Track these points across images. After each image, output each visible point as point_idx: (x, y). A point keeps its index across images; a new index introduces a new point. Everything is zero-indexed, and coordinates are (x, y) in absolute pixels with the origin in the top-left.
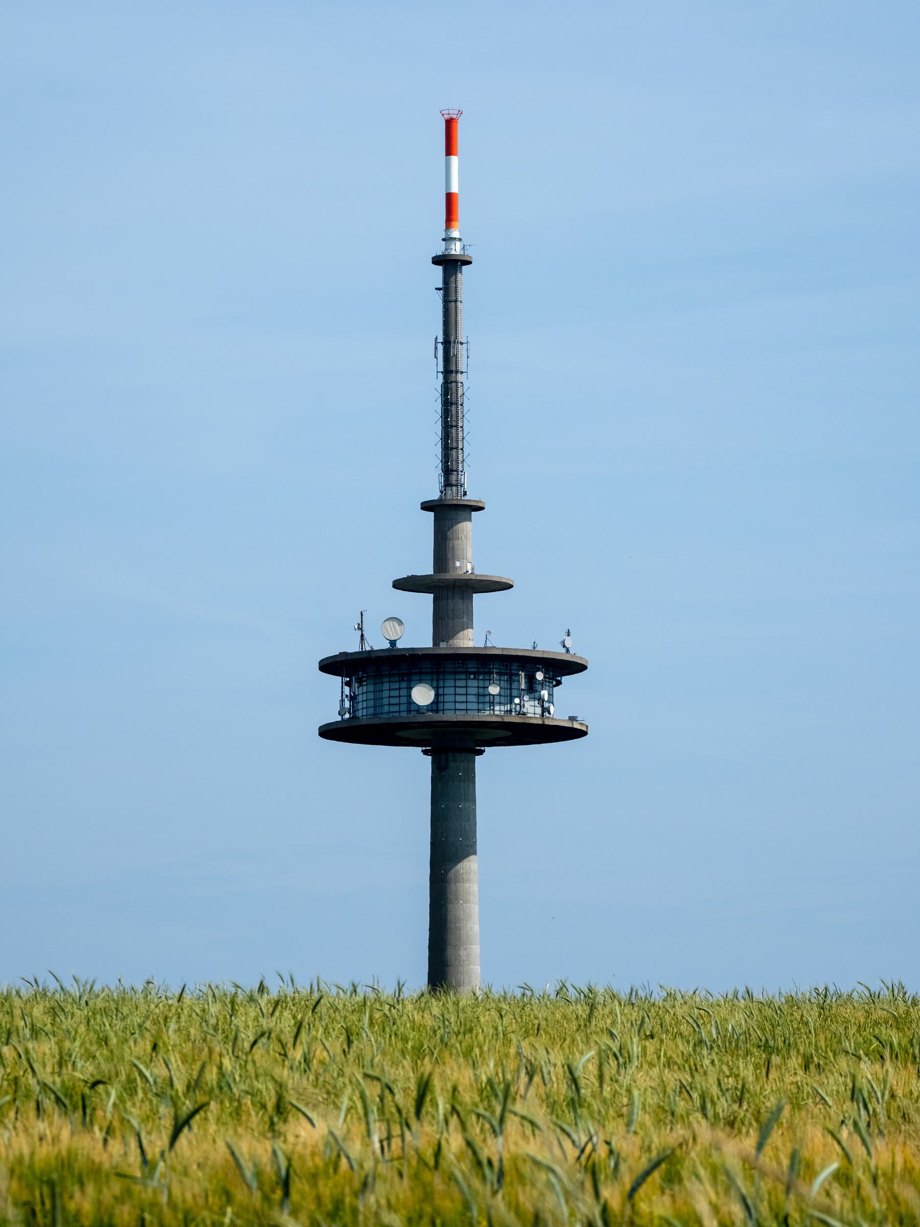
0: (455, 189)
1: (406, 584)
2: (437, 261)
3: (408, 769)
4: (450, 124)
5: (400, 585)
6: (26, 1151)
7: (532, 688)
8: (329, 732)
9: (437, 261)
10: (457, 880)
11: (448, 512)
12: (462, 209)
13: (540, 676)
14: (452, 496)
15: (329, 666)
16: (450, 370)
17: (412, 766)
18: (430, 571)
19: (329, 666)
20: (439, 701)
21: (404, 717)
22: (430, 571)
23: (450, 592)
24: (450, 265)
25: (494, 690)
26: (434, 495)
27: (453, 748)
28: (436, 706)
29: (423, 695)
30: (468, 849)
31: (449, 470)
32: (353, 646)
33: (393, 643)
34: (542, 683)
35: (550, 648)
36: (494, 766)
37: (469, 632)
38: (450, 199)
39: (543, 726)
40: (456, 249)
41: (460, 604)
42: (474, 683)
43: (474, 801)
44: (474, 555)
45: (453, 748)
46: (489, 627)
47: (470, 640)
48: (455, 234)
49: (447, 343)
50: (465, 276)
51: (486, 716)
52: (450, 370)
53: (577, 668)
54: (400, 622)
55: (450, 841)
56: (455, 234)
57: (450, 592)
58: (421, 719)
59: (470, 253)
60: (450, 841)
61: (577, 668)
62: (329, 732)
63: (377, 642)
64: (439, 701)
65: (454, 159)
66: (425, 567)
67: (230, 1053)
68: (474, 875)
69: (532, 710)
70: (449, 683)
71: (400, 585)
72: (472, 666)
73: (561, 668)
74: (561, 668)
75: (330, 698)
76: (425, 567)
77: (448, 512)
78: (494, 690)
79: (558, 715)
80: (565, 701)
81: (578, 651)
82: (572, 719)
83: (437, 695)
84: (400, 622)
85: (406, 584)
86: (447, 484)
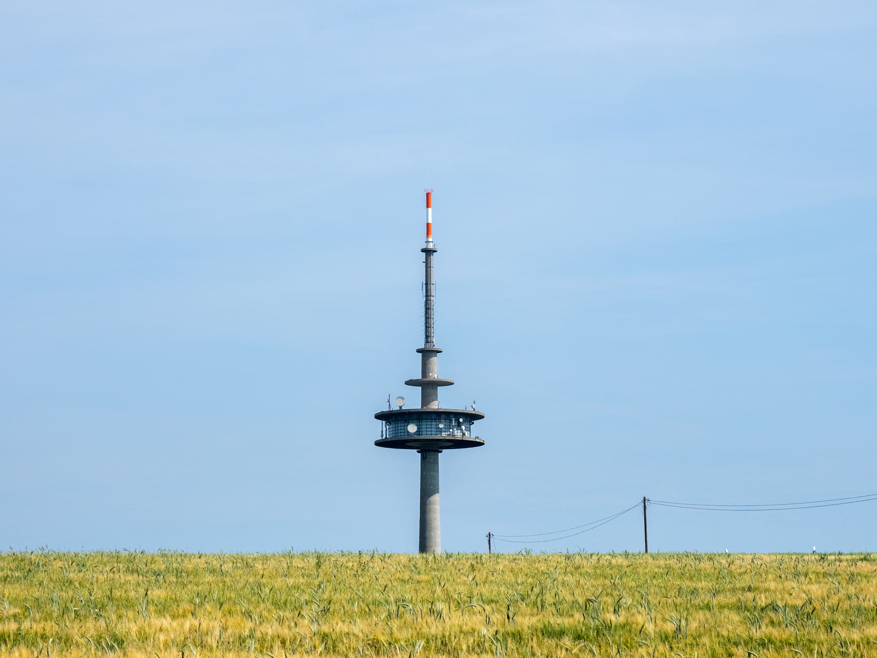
0: (430, 221)
1: (410, 383)
2: (423, 251)
3: (410, 460)
4: (428, 195)
5: (408, 383)
6: (546, 639)
7: (459, 425)
8: (379, 444)
9: (423, 251)
10: (430, 504)
11: (427, 353)
12: (433, 229)
13: (461, 420)
14: (429, 347)
15: (379, 416)
16: (428, 296)
17: (413, 457)
18: (420, 377)
19: (379, 416)
20: (424, 431)
21: (406, 437)
22: (420, 377)
23: (428, 386)
24: (428, 252)
25: (441, 426)
26: (422, 346)
27: (429, 449)
28: (419, 432)
29: (412, 428)
30: (436, 490)
31: (428, 337)
32: (386, 409)
33: (400, 407)
34: (463, 423)
35: (470, 410)
36: (446, 457)
37: (436, 402)
38: (428, 224)
39: (462, 441)
40: (431, 246)
41: (432, 391)
42: (434, 423)
43: (438, 472)
44: (438, 370)
45: (429, 449)
46: (444, 401)
47: (434, 406)
48: (430, 240)
49: (426, 284)
50: (434, 258)
51: (438, 437)
52: (428, 296)
53: (480, 417)
54: (403, 398)
55: (428, 487)
56: (430, 240)
57: (428, 386)
58: (412, 438)
59: (437, 248)
60: (428, 487)
61: (480, 417)
62: (379, 444)
63: (395, 407)
64: (424, 431)
65: (430, 209)
66: (419, 376)
67: (324, 582)
68: (437, 500)
69: (458, 434)
70: (424, 423)
71: (408, 383)
72: (434, 416)
73: (472, 418)
74: (472, 418)
75: (380, 430)
76: (419, 376)
77: (427, 353)
78: (441, 426)
79: (468, 437)
80: (475, 431)
81: (479, 411)
82: (477, 438)
83: (418, 428)
84: (403, 398)
85: (410, 383)
86: (427, 342)
